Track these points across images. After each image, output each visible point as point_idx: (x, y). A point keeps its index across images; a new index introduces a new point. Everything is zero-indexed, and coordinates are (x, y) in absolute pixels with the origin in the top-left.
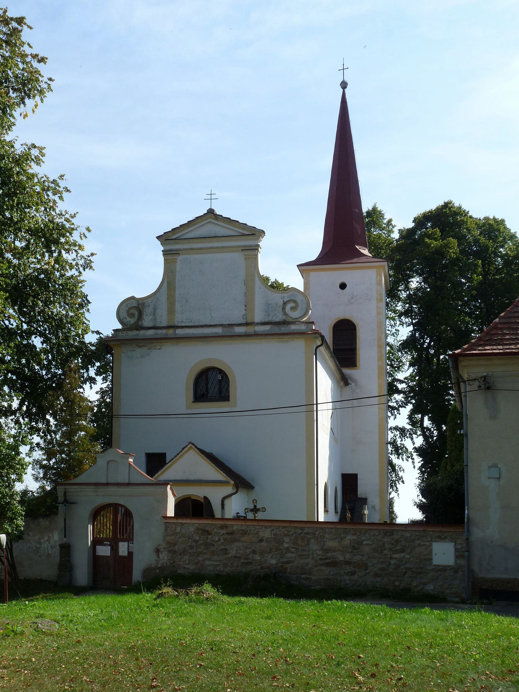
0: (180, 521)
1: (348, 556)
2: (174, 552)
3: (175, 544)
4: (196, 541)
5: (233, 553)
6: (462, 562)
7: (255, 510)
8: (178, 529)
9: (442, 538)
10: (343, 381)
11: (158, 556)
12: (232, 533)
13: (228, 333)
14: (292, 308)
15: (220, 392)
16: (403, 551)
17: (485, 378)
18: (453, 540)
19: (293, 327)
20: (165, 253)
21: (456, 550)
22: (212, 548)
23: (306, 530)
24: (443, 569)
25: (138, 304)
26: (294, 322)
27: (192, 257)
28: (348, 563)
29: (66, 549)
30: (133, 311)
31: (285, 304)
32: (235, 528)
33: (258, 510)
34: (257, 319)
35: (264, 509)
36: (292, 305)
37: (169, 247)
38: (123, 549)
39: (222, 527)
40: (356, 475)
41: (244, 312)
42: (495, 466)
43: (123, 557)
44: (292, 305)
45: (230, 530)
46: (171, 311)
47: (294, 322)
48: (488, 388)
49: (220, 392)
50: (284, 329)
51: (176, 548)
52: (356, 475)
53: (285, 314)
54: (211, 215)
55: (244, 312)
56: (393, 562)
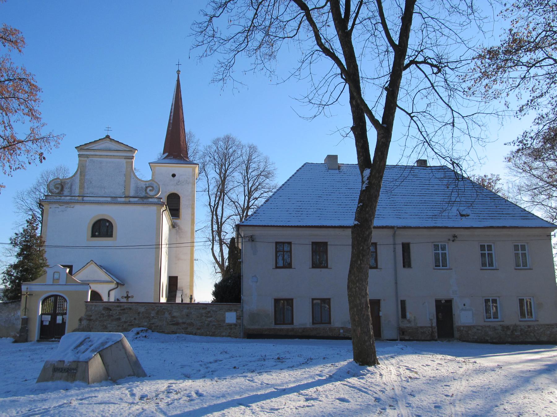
0: (94, 304)
1: (184, 320)
2: (90, 320)
3: (91, 316)
4: (103, 314)
5: (123, 320)
6: (239, 321)
7: (127, 297)
8: (93, 308)
9: (230, 310)
10: (173, 226)
11: (81, 322)
12: (124, 310)
13: (114, 200)
14: (150, 190)
15: (107, 232)
16: (211, 317)
17: (252, 236)
18: (236, 311)
19: (150, 200)
20: (80, 156)
21: (237, 316)
22: (112, 318)
23: (163, 307)
24: (230, 325)
25: (61, 182)
26: (152, 197)
27: (95, 159)
28: (184, 323)
29: (26, 322)
30: (58, 186)
31: (147, 187)
32: (125, 307)
33: (129, 297)
34: (131, 195)
35: (132, 297)
36: (151, 188)
37: (81, 153)
38: (59, 319)
39: (118, 306)
40: (177, 277)
41: (124, 191)
42: (255, 276)
43: (59, 324)
44: (151, 188)
45: (122, 308)
46: (82, 187)
47: (152, 197)
48: (253, 241)
49: (107, 232)
50: (145, 200)
51: (92, 318)
52: (177, 277)
53: (147, 193)
54: (108, 139)
55: (124, 191)
56: (206, 322)
